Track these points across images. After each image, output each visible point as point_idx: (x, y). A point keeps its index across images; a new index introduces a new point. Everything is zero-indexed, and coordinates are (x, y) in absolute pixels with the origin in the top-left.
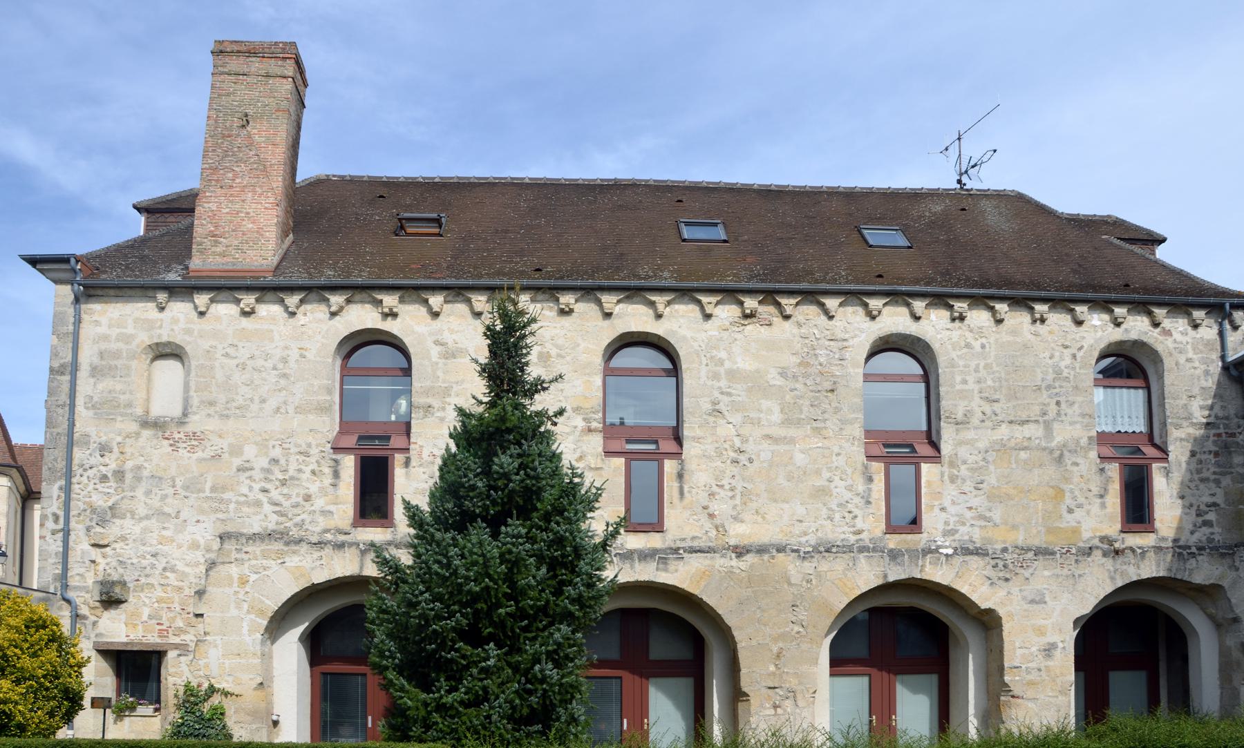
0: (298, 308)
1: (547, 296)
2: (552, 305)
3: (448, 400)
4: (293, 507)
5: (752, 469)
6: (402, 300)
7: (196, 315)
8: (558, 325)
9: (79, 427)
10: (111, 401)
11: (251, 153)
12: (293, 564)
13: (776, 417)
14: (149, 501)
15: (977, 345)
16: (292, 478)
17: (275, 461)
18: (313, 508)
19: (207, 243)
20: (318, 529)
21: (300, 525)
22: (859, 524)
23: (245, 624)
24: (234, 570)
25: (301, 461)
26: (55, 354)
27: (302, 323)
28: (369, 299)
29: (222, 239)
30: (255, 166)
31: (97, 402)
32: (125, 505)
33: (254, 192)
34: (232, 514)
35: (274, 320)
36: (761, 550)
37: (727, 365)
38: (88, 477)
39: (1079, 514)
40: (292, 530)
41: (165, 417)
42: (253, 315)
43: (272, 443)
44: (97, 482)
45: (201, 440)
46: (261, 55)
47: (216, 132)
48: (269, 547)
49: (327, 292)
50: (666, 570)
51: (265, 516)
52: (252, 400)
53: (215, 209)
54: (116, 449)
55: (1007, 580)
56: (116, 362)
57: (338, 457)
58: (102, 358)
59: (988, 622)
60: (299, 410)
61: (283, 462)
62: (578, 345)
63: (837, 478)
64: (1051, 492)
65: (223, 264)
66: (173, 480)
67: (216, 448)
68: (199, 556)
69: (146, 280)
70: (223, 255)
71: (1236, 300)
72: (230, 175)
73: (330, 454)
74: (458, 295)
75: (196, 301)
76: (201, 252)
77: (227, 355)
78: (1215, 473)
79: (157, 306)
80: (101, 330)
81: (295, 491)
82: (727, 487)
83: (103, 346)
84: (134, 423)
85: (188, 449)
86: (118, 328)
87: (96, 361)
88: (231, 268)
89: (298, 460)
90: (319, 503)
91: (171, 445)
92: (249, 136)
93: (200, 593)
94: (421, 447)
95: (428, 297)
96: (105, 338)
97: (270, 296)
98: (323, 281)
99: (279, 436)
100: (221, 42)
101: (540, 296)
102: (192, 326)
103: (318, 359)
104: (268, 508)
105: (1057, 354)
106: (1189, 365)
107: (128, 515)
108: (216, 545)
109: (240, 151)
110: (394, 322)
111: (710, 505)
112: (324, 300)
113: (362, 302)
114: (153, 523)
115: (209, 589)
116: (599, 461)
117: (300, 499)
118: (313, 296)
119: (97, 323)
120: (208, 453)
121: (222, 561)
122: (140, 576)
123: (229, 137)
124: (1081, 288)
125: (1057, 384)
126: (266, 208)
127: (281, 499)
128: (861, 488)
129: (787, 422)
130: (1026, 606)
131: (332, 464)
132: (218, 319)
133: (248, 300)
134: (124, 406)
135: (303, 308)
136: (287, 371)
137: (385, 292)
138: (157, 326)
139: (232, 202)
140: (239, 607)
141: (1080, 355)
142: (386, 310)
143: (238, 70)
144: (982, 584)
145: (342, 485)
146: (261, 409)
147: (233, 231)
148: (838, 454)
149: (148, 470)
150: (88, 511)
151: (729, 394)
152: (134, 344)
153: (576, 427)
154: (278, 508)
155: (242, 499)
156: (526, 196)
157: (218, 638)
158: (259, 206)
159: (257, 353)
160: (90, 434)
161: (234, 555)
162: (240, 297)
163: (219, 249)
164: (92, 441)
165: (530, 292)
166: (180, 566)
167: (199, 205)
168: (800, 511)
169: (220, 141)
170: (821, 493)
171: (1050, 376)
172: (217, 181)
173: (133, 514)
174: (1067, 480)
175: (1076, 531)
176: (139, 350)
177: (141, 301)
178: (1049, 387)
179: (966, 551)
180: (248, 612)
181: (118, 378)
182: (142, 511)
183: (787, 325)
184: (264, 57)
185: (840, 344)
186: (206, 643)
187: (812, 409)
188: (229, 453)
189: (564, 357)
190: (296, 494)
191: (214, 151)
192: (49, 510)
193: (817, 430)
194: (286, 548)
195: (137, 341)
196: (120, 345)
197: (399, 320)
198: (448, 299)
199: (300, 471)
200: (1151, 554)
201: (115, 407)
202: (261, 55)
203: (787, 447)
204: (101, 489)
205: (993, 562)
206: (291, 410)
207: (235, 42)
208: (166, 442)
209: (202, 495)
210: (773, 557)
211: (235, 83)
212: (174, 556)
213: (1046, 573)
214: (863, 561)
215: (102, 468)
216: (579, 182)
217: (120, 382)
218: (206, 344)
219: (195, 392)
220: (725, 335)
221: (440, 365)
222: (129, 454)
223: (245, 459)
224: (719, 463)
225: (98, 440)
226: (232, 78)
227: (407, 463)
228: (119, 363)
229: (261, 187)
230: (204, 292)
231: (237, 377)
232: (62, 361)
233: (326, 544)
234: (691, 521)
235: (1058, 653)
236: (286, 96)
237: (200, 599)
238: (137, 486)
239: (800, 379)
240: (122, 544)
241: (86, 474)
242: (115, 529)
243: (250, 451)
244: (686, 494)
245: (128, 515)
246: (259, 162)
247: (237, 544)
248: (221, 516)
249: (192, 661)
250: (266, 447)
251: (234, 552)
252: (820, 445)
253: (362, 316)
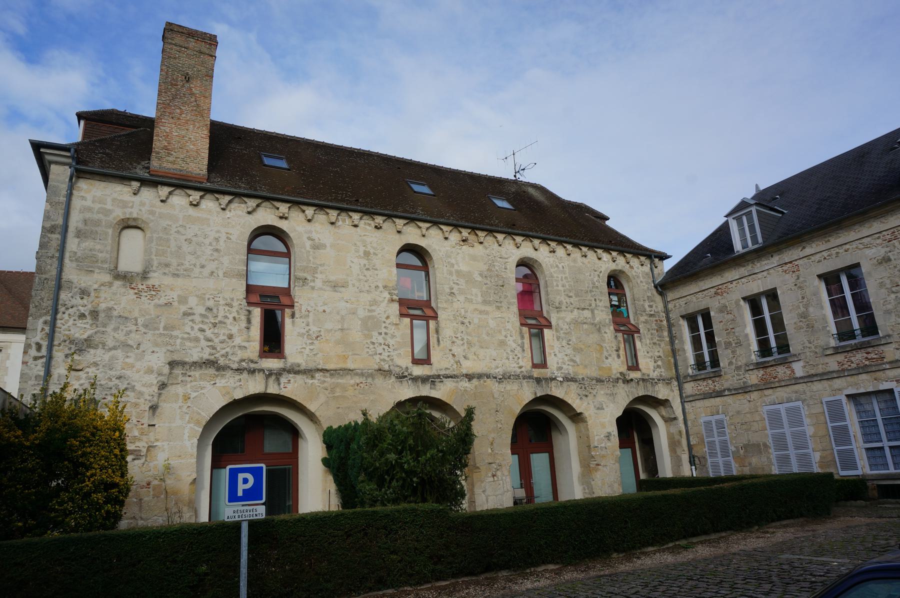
3: (316, 275)
4: (221, 342)
5: (471, 327)
8: (374, 236)
9: (66, 276)
10: (91, 257)
12: (221, 385)
13: (480, 299)
14: (116, 335)
15: (560, 266)
16: (220, 322)
17: (209, 309)
18: (233, 344)
19: (163, 153)
20: (237, 359)
21: (226, 355)
22: (521, 364)
23: (186, 431)
24: (179, 390)
25: (226, 310)
26: (47, 217)
27: (228, 216)
28: (271, 206)
31: (79, 257)
32: (97, 339)
34: (178, 347)
35: (210, 212)
36: (480, 376)
37: (456, 267)
38: (69, 315)
39: (610, 360)
40: (219, 360)
41: (131, 272)
42: (197, 208)
43: (207, 296)
44: (77, 318)
45: (158, 291)
48: (206, 372)
50: (435, 389)
51: (202, 349)
52: (195, 265)
53: (168, 131)
54: (93, 294)
55: (587, 396)
56: (96, 229)
57: (251, 308)
58: (85, 224)
59: (576, 417)
60: (226, 274)
61: (215, 311)
62: (384, 249)
63: (509, 335)
64: (598, 347)
66: (136, 319)
67: (169, 297)
68: (153, 379)
70: (173, 163)
71: (656, 254)
72: (178, 111)
73: (245, 306)
77: (178, 232)
78: (658, 340)
80: (88, 203)
81: (223, 331)
82: (460, 338)
83: (88, 215)
84: (108, 275)
85: (149, 297)
87: (81, 226)
89: (224, 309)
90: (238, 340)
91: (136, 293)
92: (190, 89)
93: (154, 408)
94: (301, 305)
96: (89, 209)
99: (212, 292)
103: (239, 241)
104: (204, 343)
105: (592, 274)
106: (642, 284)
107: (101, 346)
108: (166, 370)
111: (453, 348)
114: (119, 353)
115: (161, 404)
116: (398, 319)
117: (225, 337)
119: (83, 198)
120: (163, 301)
121: (172, 382)
122: (106, 395)
124: (615, 244)
125: (594, 290)
127: (212, 336)
128: (520, 342)
129: (485, 302)
130: (596, 411)
131: (247, 313)
133: (196, 195)
134: (102, 261)
136: (218, 247)
140: (182, 418)
141: (601, 275)
143: (181, 44)
144: (577, 398)
145: (252, 328)
146: (201, 272)
147: (180, 148)
148: (508, 322)
149: (117, 312)
150: (67, 342)
151: (458, 284)
152: (111, 218)
153: (385, 298)
154: (210, 344)
155: (186, 336)
157: (165, 443)
158: (198, 135)
159: (199, 233)
160: (73, 281)
161: (180, 378)
163: (171, 159)
164: (74, 286)
166: (138, 387)
168: (494, 353)
170: (502, 343)
171: (591, 286)
172: (170, 113)
173: (104, 345)
174: (604, 341)
175: (610, 369)
176: (115, 222)
178: (591, 291)
179: (568, 379)
180: (189, 422)
181: (98, 241)
182: (110, 343)
183: (480, 247)
185: (504, 260)
186: (157, 448)
187: (495, 296)
188: (178, 302)
189: (377, 255)
190: (223, 332)
191: (166, 92)
192: (33, 340)
193: (498, 308)
194: (217, 373)
195: (114, 215)
196: (101, 216)
199: (226, 317)
200: (641, 382)
201: (94, 262)
203: (485, 316)
204: (79, 325)
205: (580, 386)
206: (221, 274)
208: (132, 291)
209: (157, 332)
210: (485, 382)
211: (179, 52)
212: (133, 378)
213: (602, 392)
214: (525, 384)
215: (80, 308)
217: (99, 243)
218: (164, 223)
219: (156, 256)
220: (454, 250)
221: (311, 253)
222: (103, 298)
223: (189, 307)
224: (455, 324)
225: (79, 286)
226: (178, 48)
227: (293, 316)
228: (99, 229)
231: (186, 248)
232: (53, 223)
233: (244, 370)
234: (444, 359)
235: (612, 438)
237: (154, 414)
238: (108, 324)
239: (488, 278)
240: (94, 369)
241: (67, 312)
242: (92, 355)
243: (193, 301)
244: (441, 342)
245: (101, 346)
246: (198, 106)
247: (183, 369)
248: (170, 348)
249: (144, 464)
250: (204, 299)
251: (181, 376)
252: (500, 316)
253: (266, 216)
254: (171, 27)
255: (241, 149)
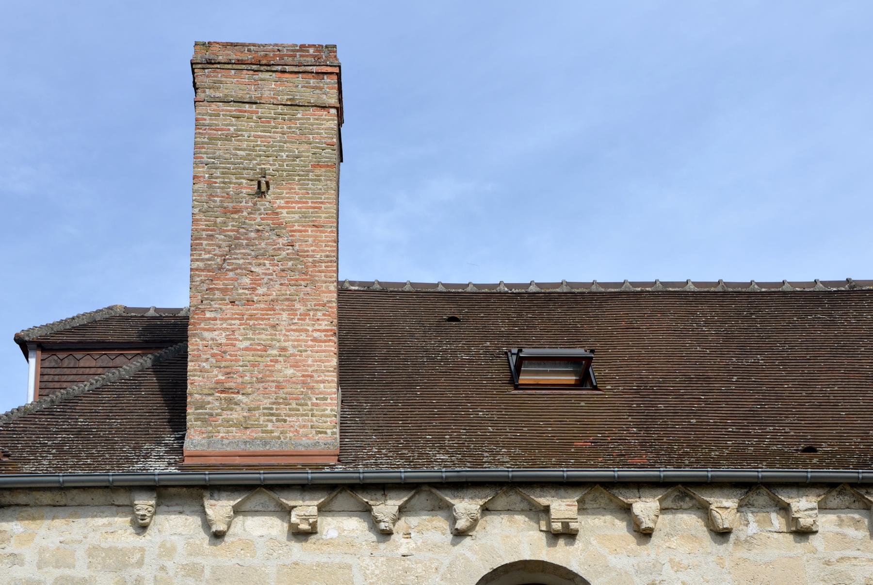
0: (395, 521)
1: (847, 500)
2: (857, 516)
6: (582, 509)
7: (207, 538)
11: (280, 241)
19: (214, 403)
27: (403, 550)
28: (524, 506)
29: (240, 397)
30: (290, 263)
33: (292, 311)
42: (313, 538)
46: (279, 68)
47: (212, 204)
49: (449, 493)
53: (224, 341)
65: (245, 443)
69: (113, 475)
72: (246, 280)
74: (683, 496)
75: (209, 511)
76: (204, 421)
79: (134, 523)
86: (58, 567)
88: (260, 449)
95: (630, 501)
97: (343, 500)
98: (437, 472)
100: (207, 45)
101: (835, 500)
102: (198, 560)
109: (260, 238)
110: (571, 548)
112: (440, 508)
113: (509, 511)
118: (422, 499)
123: (236, 212)
126: (315, 340)
132: (248, 545)
135: (402, 523)
137: (553, 492)
138: (134, 560)
139: (253, 328)
142: (557, 526)
147: (260, 381)
156: (704, 315)
158: (303, 336)
162: (291, 503)
163: (236, 415)
165: (817, 491)
167: (194, 335)
169: (219, 220)
177: (102, 515)
184: (284, 72)
191: (211, 237)
197: (579, 544)
198: (665, 505)
202: (279, 68)
207: (232, 44)
216: (786, 288)
226: (232, 108)
229: (303, 301)
230: (224, 494)
236: (329, 141)
246: (299, 255)
254: (208, 55)
255: (454, 352)
